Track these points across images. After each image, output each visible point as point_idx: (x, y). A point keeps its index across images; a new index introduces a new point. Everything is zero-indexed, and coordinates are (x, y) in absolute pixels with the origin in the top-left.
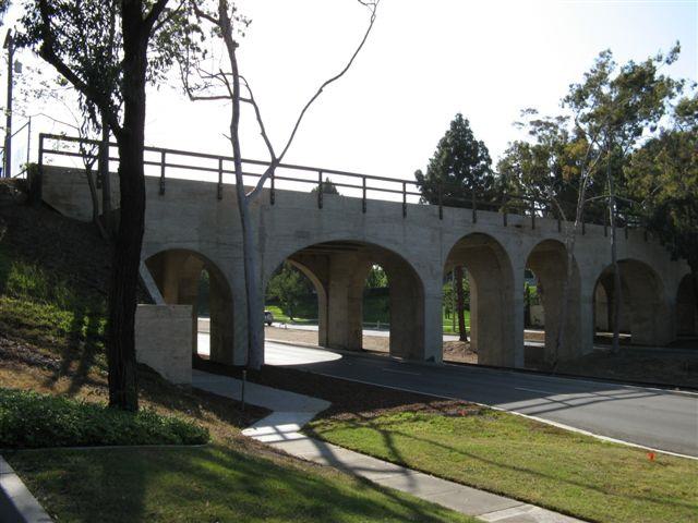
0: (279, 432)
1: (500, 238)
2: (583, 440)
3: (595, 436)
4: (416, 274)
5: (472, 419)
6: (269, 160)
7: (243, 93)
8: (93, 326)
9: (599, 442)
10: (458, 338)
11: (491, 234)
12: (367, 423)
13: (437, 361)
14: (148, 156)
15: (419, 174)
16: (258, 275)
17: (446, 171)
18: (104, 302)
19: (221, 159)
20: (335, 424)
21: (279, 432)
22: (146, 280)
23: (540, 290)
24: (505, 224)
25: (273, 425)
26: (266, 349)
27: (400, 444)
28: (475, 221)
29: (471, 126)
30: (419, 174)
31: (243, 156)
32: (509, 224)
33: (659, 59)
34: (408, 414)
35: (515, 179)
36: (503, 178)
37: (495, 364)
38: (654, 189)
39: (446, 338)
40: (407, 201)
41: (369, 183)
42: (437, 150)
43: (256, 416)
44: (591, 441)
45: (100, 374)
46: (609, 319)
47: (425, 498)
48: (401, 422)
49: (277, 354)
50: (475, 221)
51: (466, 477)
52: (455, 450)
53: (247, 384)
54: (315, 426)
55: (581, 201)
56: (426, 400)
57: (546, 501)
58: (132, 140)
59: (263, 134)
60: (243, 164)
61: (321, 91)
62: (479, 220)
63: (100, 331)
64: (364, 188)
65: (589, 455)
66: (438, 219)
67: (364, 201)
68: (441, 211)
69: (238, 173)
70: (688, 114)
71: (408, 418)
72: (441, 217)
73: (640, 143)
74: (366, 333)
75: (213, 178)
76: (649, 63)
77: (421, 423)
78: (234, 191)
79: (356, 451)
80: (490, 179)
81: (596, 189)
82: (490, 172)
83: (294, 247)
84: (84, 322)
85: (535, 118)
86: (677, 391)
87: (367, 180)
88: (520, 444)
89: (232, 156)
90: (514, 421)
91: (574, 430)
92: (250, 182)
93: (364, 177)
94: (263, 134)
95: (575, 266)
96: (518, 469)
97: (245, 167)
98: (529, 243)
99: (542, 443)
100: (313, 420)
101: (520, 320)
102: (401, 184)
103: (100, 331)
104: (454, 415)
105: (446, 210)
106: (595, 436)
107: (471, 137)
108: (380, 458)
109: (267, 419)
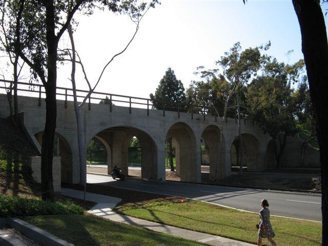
0: (103, 212)
1: (190, 124)
2: (233, 211)
3: (53, 238)
4: (154, 141)
5: (185, 204)
6: (89, 90)
7: (77, 59)
8: (17, 167)
9: (240, 212)
10: (170, 170)
11: (186, 123)
12: (140, 207)
13: (163, 180)
14: (58, 91)
15: (151, 95)
16: (83, 142)
17: (164, 94)
18: (20, 156)
19: (66, 89)
20: (127, 208)
21: (103, 212)
22: (37, 146)
23: (207, 147)
24: (192, 118)
25: (100, 209)
26: (87, 177)
27: (157, 214)
28: (179, 117)
29: (176, 74)
30: (151, 95)
31: (77, 88)
32: (194, 118)
33: (262, 48)
34: (156, 203)
35: (195, 97)
36: (190, 97)
37: (188, 181)
38: (258, 103)
39: (167, 170)
40: (132, 107)
41: (133, 100)
42: (160, 84)
43: (91, 205)
44: (235, 211)
45: (23, 188)
46: (238, 160)
47: (174, 235)
48: (155, 206)
49: (91, 179)
50: (179, 117)
51: (188, 227)
52: (181, 216)
53: (87, 193)
54: (118, 209)
55: (226, 107)
56: (164, 197)
57: (222, 234)
58: (51, 86)
59: (86, 78)
60: (77, 92)
61: (112, 59)
62: (181, 117)
63: (20, 169)
64: (130, 103)
65: (237, 216)
66: (163, 116)
67: (130, 108)
68: (164, 113)
69: (75, 96)
70: (270, 69)
71: (158, 205)
72: (164, 115)
73: (250, 81)
74: (129, 168)
75: (145, 107)
76: (257, 49)
77: (164, 206)
78: (73, 104)
79: (139, 218)
80: (184, 98)
81: (231, 102)
82: (184, 94)
83: (99, 129)
84: (12, 165)
85: (203, 70)
86: (269, 190)
87: (132, 99)
88: (208, 213)
89: (72, 88)
90: (203, 204)
91: (229, 207)
92: (80, 100)
93: (130, 98)
94: (86, 78)
95: (223, 137)
96: (209, 222)
97: (78, 93)
98: (203, 127)
99: (217, 213)
100: (116, 206)
101: (199, 162)
102: (129, 98)
103: (20, 169)
104: (177, 203)
105: (166, 112)
106: (53, 238)
107: (175, 78)
108: (150, 221)
109: (96, 206)
